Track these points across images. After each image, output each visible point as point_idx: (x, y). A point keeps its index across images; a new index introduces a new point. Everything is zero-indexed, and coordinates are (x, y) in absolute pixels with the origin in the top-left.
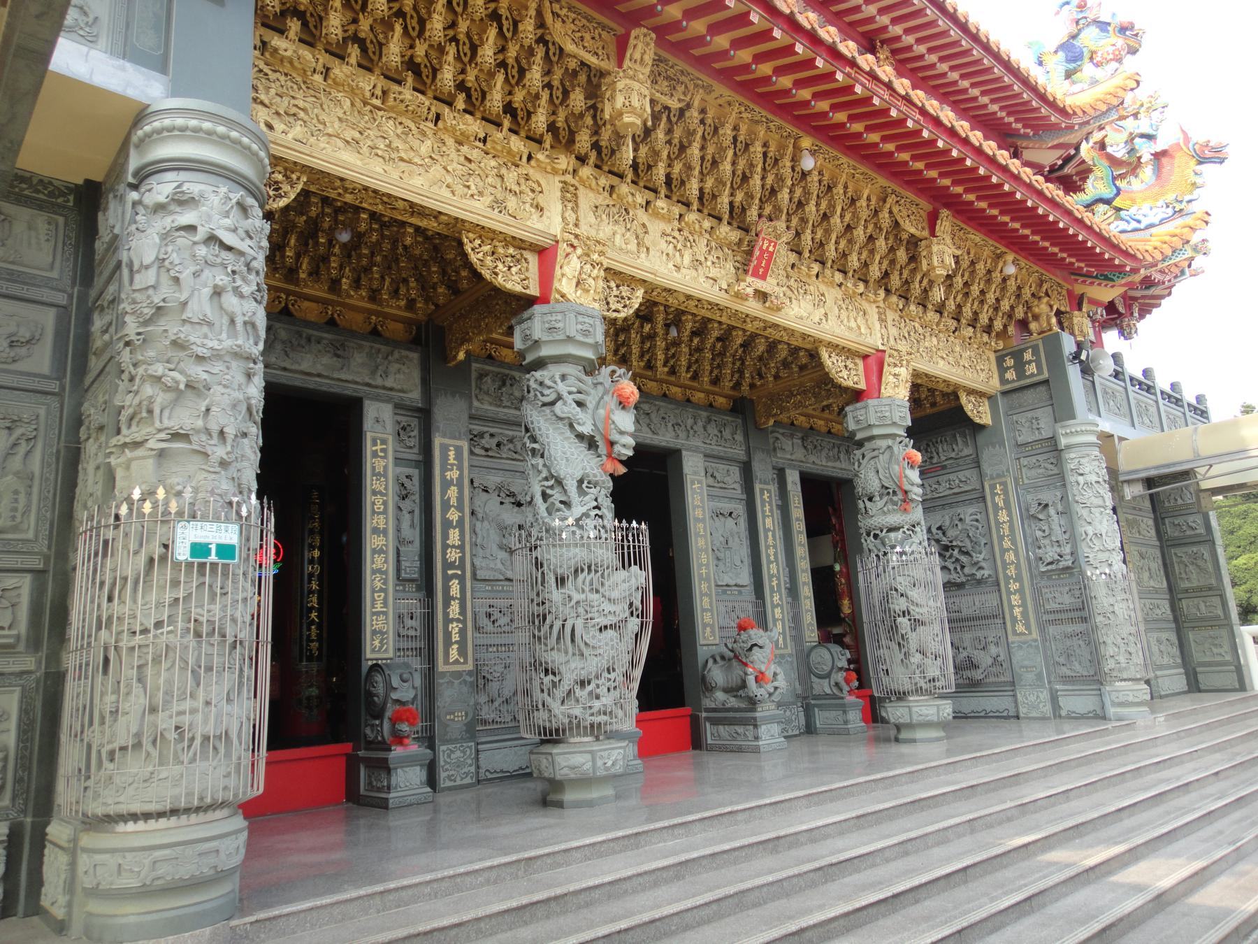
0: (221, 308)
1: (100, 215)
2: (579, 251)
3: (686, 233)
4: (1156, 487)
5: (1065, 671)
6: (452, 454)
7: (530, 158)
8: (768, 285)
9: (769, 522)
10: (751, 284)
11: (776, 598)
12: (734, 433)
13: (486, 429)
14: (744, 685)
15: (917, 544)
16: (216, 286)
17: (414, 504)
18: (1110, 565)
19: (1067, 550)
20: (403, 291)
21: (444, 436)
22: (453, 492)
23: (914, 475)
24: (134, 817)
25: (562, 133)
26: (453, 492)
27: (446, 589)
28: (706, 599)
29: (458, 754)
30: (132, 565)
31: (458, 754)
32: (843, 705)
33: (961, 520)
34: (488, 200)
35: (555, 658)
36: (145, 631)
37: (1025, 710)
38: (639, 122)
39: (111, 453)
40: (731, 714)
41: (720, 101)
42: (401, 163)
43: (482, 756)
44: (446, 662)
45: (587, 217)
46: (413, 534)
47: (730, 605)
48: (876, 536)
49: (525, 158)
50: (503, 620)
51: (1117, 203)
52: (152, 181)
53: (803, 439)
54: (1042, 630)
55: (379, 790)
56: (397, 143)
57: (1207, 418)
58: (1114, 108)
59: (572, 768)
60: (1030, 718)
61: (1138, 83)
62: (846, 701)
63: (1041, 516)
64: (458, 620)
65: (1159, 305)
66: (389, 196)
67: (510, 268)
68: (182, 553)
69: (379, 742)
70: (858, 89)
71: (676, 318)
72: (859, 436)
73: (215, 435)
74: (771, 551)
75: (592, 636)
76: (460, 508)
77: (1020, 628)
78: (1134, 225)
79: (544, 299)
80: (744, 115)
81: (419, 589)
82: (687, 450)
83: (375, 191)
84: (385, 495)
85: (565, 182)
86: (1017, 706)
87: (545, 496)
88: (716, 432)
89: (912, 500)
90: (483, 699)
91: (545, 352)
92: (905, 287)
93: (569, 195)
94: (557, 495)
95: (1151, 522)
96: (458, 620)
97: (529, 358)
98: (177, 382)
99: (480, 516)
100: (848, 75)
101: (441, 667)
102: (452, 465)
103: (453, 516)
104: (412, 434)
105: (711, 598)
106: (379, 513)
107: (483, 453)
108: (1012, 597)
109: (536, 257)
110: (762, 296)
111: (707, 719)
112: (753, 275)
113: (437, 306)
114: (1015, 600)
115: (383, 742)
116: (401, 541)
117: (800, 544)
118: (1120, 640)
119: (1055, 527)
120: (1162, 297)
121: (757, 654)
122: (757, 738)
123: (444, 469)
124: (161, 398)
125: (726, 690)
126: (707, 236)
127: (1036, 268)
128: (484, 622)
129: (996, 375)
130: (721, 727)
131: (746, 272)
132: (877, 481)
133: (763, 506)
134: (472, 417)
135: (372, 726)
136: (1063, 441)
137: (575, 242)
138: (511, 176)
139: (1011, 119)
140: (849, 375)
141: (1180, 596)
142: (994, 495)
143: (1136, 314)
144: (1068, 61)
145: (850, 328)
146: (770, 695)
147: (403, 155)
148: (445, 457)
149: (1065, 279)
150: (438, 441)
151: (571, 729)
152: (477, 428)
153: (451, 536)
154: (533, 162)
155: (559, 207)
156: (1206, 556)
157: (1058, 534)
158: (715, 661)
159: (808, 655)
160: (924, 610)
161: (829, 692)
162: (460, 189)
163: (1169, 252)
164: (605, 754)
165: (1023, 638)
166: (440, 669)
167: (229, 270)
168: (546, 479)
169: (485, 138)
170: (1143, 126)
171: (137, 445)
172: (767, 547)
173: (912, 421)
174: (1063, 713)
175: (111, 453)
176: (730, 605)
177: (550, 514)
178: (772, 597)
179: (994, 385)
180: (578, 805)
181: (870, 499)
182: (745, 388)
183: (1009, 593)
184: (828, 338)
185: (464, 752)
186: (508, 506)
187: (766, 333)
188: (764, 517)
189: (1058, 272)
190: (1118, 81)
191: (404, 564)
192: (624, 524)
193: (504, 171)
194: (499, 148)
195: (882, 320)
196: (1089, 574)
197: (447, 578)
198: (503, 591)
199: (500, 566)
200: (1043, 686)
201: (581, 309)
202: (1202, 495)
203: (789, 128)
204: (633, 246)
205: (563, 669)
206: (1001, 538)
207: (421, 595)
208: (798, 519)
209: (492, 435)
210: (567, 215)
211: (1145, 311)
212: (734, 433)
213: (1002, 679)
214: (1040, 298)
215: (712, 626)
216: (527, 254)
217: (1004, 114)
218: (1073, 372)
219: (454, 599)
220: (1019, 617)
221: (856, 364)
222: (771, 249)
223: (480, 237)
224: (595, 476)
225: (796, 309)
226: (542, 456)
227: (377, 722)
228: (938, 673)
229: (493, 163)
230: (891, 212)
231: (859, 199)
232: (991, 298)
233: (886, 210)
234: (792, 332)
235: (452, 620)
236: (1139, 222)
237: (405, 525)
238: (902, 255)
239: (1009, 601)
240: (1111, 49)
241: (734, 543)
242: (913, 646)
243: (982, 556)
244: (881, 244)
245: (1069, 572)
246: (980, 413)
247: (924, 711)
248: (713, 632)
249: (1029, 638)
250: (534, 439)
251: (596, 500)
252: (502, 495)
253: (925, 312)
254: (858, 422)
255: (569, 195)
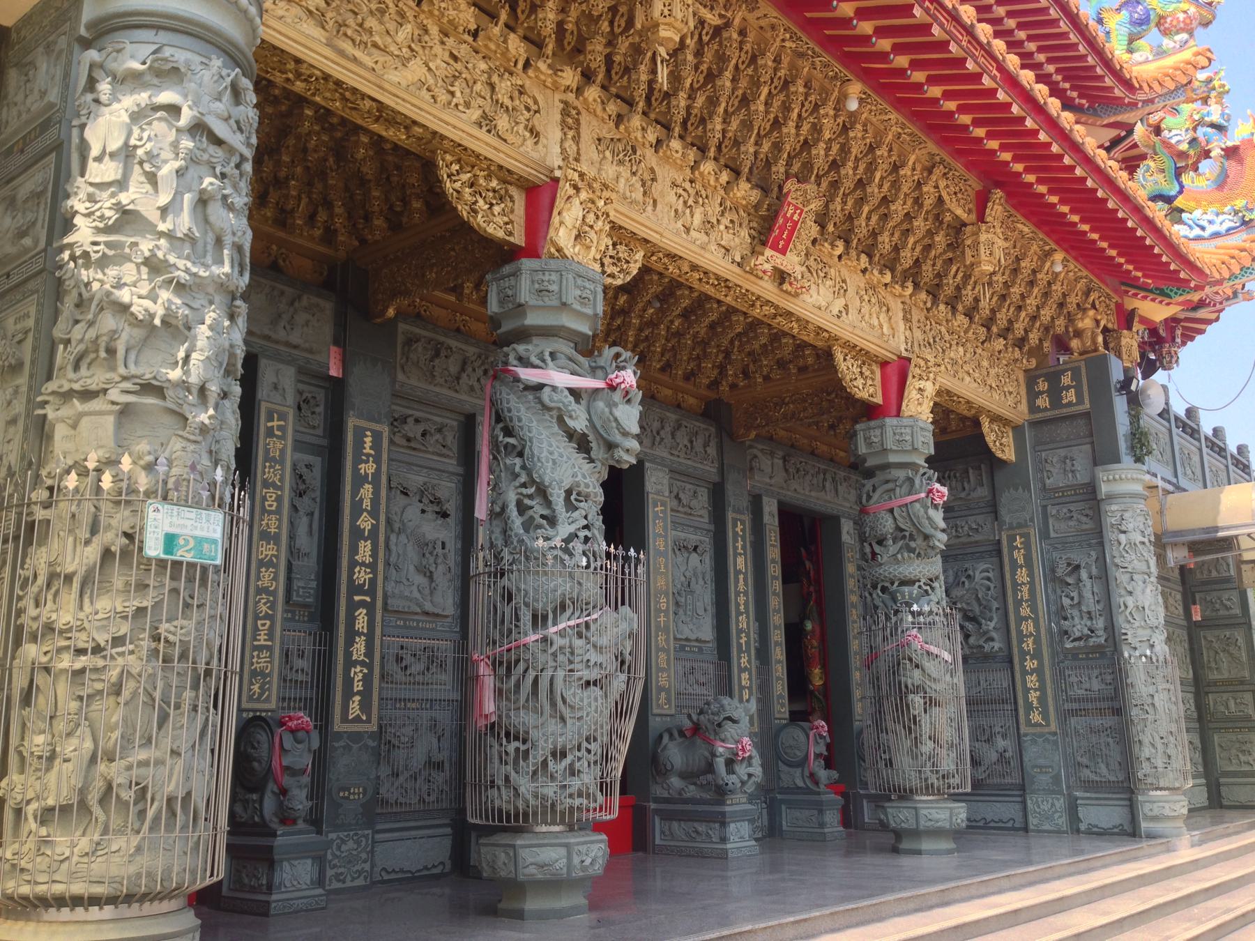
0: (206, 221)
1: (13, 76)
2: (584, 195)
3: (698, 186)
4: (187, 571)
5: (1086, 773)
6: (368, 440)
7: (527, 65)
8: (791, 262)
9: (740, 561)
10: (769, 259)
11: (744, 660)
12: (706, 445)
13: (410, 412)
14: (710, 768)
15: (934, 603)
16: (202, 192)
17: (312, 503)
18: (1152, 646)
19: (1100, 623)
20: (322, 216)
21: (360, 416)
22: (367, 491)
23: (938, 517)
24: (95, 901)
25: (568, 37)
26: (367, 491)
27: (351, 620)
28: (662, 656)
29: (351, 844)
30: (79, 557)
31: (351, 844)
32: (820, 803)
33: (969, 577)
34: (476, 114)
35: (524, 719)
36: (97, 649)
37: (1035, 821)
38: (677, 39)
39: (46, 402)
40: (689, 807)
41: (763, 23)
42: (374, 50)
43: (378, 849)
44: (345, 719)
45: (589, 151)
46: (308, 543)
47: (688, 664)
48: (884, 590)
49: (520, 65)
50: (416, 668)
51: (1179, 202)
52: (124, 38)
53: (784, 459)
54: (1064, 716)
55: (253, 890)
56: (371, 23)
57: (1249, 474)
58: (1181, 87)
59: (541, 866)
60: (1039, 831)
61: (1210, 60)
62: (824, 797)
63: (1070, 580)
64: (362, 663)
65: (1202, 332)
66: (355, 91)
67: (492, 205)
68: (154, 549)
69: (256, 824)
70: (936, 30)
71: (673, 288)
72: (870, 463)
73: (195, 391)
74: (742, 599)
75: (575, 695)
76: (374, 513)
77: (1036, 717)
78: (1197, 232)
79: (531, 250)
80: (788, 44)
81: (311, 619)
82: (650, 461)
83: (339, 83)
84: (281, 488)
85: (565, 103)
86: (1025, 816)
87: (522, 508)
88: (686, 442)
89: (933, 548)
90: (384, 771)
91: (532, 320)
92: (936, 281)
93: (570, 119)
94: (538, 509)
95: (1179, 597)
96: (362, 663)
97: (507, 327)
98: (152, 316)
99: (396, 526)
100: (927, 11)
101: (338, 726)
102: (368, 455)
103: (365, 523)
104: (318, 410)
105: (668, 656)
106: (270, 513)
107: (404, 442)
108: (1028, 678)
109: (524, 196)
110: (781, 277)
111: (656, 811)
112: (773, 248)
113: (363, 242)
114: (1032, 681)
115: (264, 824)
116: (293, 551)
117: (774, 594)
118: (1157, 739)
119: (1087, 594)
120: (1209, 322)
121: (730, 730)
122: (724, 840)
123: (357, 461)
124: (127, 335)
125: (684, 776)
126: (722, 192)
127: (1085, 273)
128: (393, 667)
129: (1024, 401)
130: (675, 824)
131: (764, 244)
132: (890, 521)
133: (736, 541)
134: (395, 395)
135: (247, 801)
136: (1104, 489)
137: (580, 184)
138: (504, 86)
139: (1067, 85)
140: (865, 385)
141: (1206, 689)
142: (1012, 548)
143: (1178, 340)
144: (1133, 23)
145: (872, 327)
146: (743, 783)
147: (377, 39)
148: (359, 444)
149: (1116, 291)
150: (352, 422)
151: (544, 813)
152: (400, 410)
153: (361, 552)
154: (531, 72)
155: (558, 134)
156: (1241, 642)
157: (1090, 603)
158: (671, 735)
159: (777, 735)
160: (938, 687)
161: (800, 784)
162: (443, 97)
163: (1236, 270)
164: (583, 848)
165: (1039, 729)
166: (336, 728)
167: (218, 171)
168: (524, 485)
169: (477, 31)
170: (1214, 113)
171: (88, 395)
172: (738, 594)
173: (936, 445)
174: (1083, 827)
175: (46, 402)
176: (688, 664)
177: (527, 530)
178: (740, 658)
179: (1020, 413)
180: (543, 916)
181: (880, 543)
182: (724, 387)
183: (1025, 673)
184: (846, 335)
185: (358, 843)
186: (430, 516)
187: (774, 323)
188: (736, 555)
189: (1108, 279)
190: (1187, 55)
191: (296, 584)
192: (621, 552)
193: (495, 78)
194: (493, 47)
195: (907, 319)
196: (1126, 655)
197: (352, 607)
198: (417, 628)
199: (416, 594)
200: (1060, 792)
201: (582, 270)
202: (1244, 567)
203: (837, 67)
204: (638, 195)
205: (533, 734)
206: (1018, 603)
207: (315, 627)
208: (773, 561)
209: (417, 421)
210: (567, 145)
211: (1188, 337)
212: (706, 445)
213: (1008, 780)
214: (1085, 310)
215: (668, 691)
216: (513, 191)
217: (1059, 78)
218: (1120, 404)
219: (360, 634)
220: (1035, 703)
221: (873, 372)
222: (796, 218)
223: (459, 161)
224: (587, 486)
225: (815, 295)
226: (521, 455)
227: (255, 797)
228: (953, 767)
229: (483, 66)
230: (936, 187)
231: (903, 165)
232: (1032, 302)
233: (931, 183)
234: (804, 323)
235: (356, 663)
236: (1203, 228)
237: (302, 530)
238: (940, 239)
239: (1024, 682)
240: (1181, 16)
241: (698, 587)
242: (926, 729)
243: (992, 625)
244: (919, 224)
245: (1107, 653)
246: (1004, 447)
247: (935, 814)
248: (668, 700)
249: (1046, 730)
250: (508, 432)
251: (586, 517)
252: (425, 500)
253: (954, 314)
254: (869, 444)
255: (570, 121)
